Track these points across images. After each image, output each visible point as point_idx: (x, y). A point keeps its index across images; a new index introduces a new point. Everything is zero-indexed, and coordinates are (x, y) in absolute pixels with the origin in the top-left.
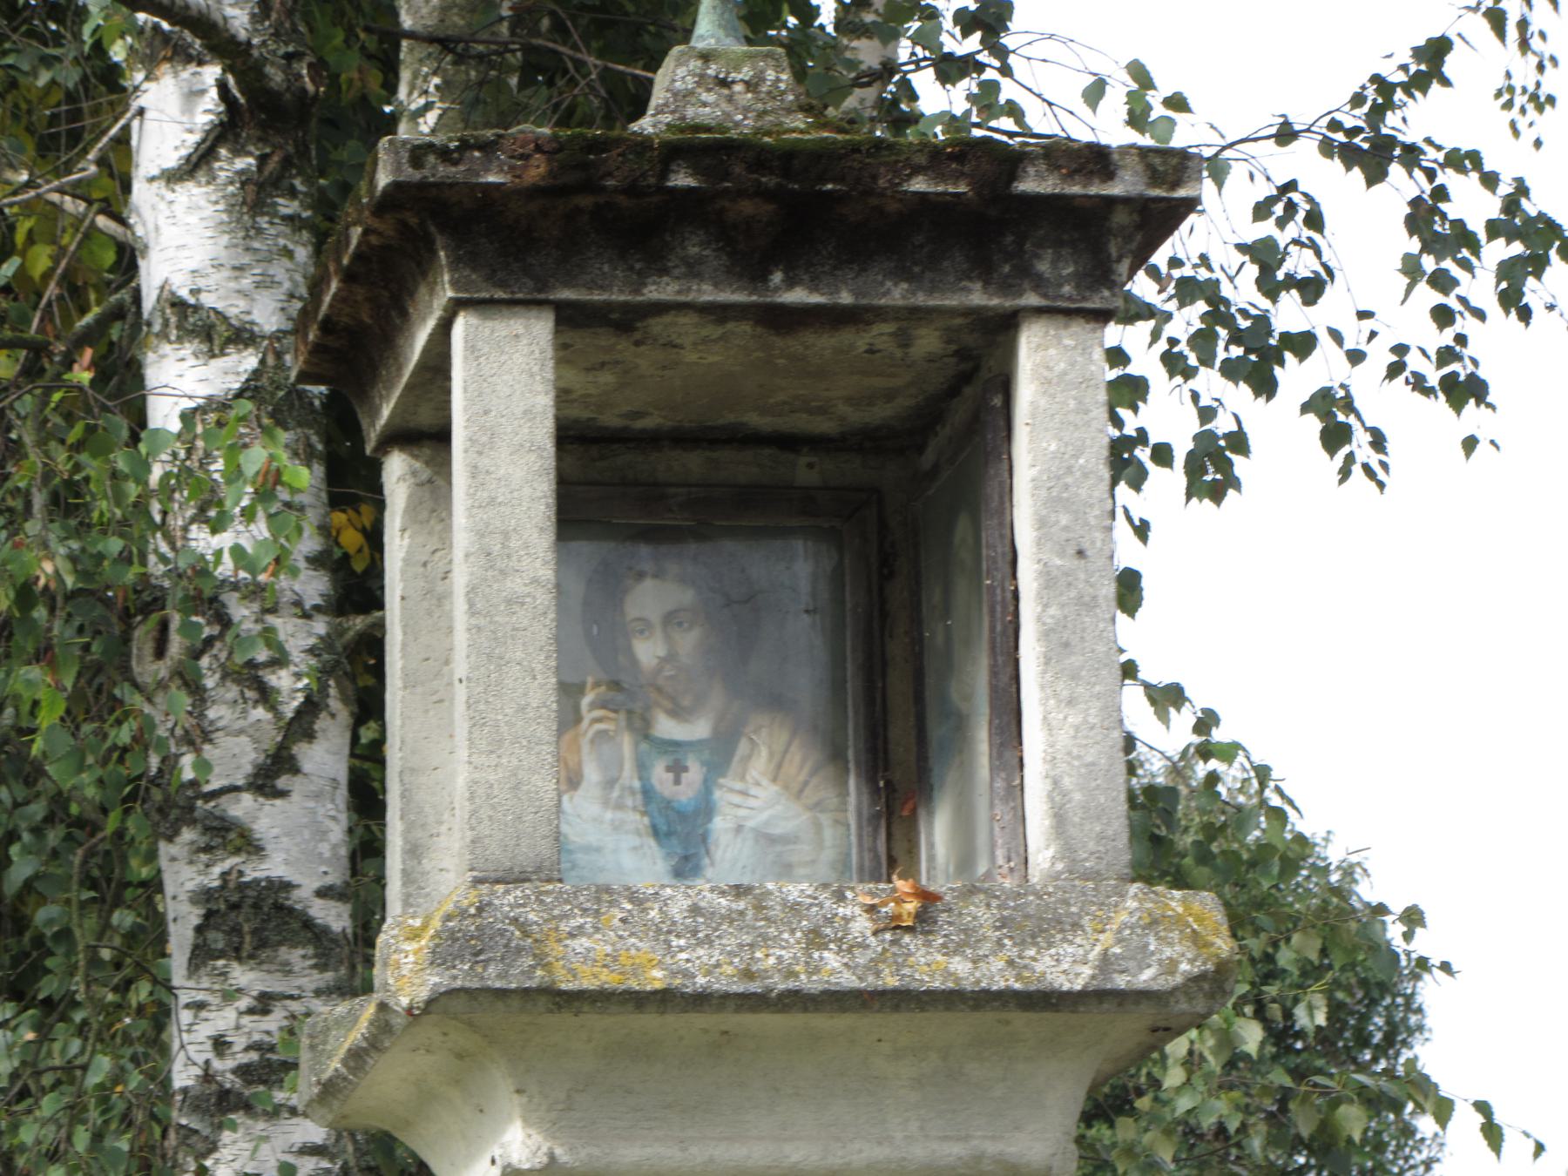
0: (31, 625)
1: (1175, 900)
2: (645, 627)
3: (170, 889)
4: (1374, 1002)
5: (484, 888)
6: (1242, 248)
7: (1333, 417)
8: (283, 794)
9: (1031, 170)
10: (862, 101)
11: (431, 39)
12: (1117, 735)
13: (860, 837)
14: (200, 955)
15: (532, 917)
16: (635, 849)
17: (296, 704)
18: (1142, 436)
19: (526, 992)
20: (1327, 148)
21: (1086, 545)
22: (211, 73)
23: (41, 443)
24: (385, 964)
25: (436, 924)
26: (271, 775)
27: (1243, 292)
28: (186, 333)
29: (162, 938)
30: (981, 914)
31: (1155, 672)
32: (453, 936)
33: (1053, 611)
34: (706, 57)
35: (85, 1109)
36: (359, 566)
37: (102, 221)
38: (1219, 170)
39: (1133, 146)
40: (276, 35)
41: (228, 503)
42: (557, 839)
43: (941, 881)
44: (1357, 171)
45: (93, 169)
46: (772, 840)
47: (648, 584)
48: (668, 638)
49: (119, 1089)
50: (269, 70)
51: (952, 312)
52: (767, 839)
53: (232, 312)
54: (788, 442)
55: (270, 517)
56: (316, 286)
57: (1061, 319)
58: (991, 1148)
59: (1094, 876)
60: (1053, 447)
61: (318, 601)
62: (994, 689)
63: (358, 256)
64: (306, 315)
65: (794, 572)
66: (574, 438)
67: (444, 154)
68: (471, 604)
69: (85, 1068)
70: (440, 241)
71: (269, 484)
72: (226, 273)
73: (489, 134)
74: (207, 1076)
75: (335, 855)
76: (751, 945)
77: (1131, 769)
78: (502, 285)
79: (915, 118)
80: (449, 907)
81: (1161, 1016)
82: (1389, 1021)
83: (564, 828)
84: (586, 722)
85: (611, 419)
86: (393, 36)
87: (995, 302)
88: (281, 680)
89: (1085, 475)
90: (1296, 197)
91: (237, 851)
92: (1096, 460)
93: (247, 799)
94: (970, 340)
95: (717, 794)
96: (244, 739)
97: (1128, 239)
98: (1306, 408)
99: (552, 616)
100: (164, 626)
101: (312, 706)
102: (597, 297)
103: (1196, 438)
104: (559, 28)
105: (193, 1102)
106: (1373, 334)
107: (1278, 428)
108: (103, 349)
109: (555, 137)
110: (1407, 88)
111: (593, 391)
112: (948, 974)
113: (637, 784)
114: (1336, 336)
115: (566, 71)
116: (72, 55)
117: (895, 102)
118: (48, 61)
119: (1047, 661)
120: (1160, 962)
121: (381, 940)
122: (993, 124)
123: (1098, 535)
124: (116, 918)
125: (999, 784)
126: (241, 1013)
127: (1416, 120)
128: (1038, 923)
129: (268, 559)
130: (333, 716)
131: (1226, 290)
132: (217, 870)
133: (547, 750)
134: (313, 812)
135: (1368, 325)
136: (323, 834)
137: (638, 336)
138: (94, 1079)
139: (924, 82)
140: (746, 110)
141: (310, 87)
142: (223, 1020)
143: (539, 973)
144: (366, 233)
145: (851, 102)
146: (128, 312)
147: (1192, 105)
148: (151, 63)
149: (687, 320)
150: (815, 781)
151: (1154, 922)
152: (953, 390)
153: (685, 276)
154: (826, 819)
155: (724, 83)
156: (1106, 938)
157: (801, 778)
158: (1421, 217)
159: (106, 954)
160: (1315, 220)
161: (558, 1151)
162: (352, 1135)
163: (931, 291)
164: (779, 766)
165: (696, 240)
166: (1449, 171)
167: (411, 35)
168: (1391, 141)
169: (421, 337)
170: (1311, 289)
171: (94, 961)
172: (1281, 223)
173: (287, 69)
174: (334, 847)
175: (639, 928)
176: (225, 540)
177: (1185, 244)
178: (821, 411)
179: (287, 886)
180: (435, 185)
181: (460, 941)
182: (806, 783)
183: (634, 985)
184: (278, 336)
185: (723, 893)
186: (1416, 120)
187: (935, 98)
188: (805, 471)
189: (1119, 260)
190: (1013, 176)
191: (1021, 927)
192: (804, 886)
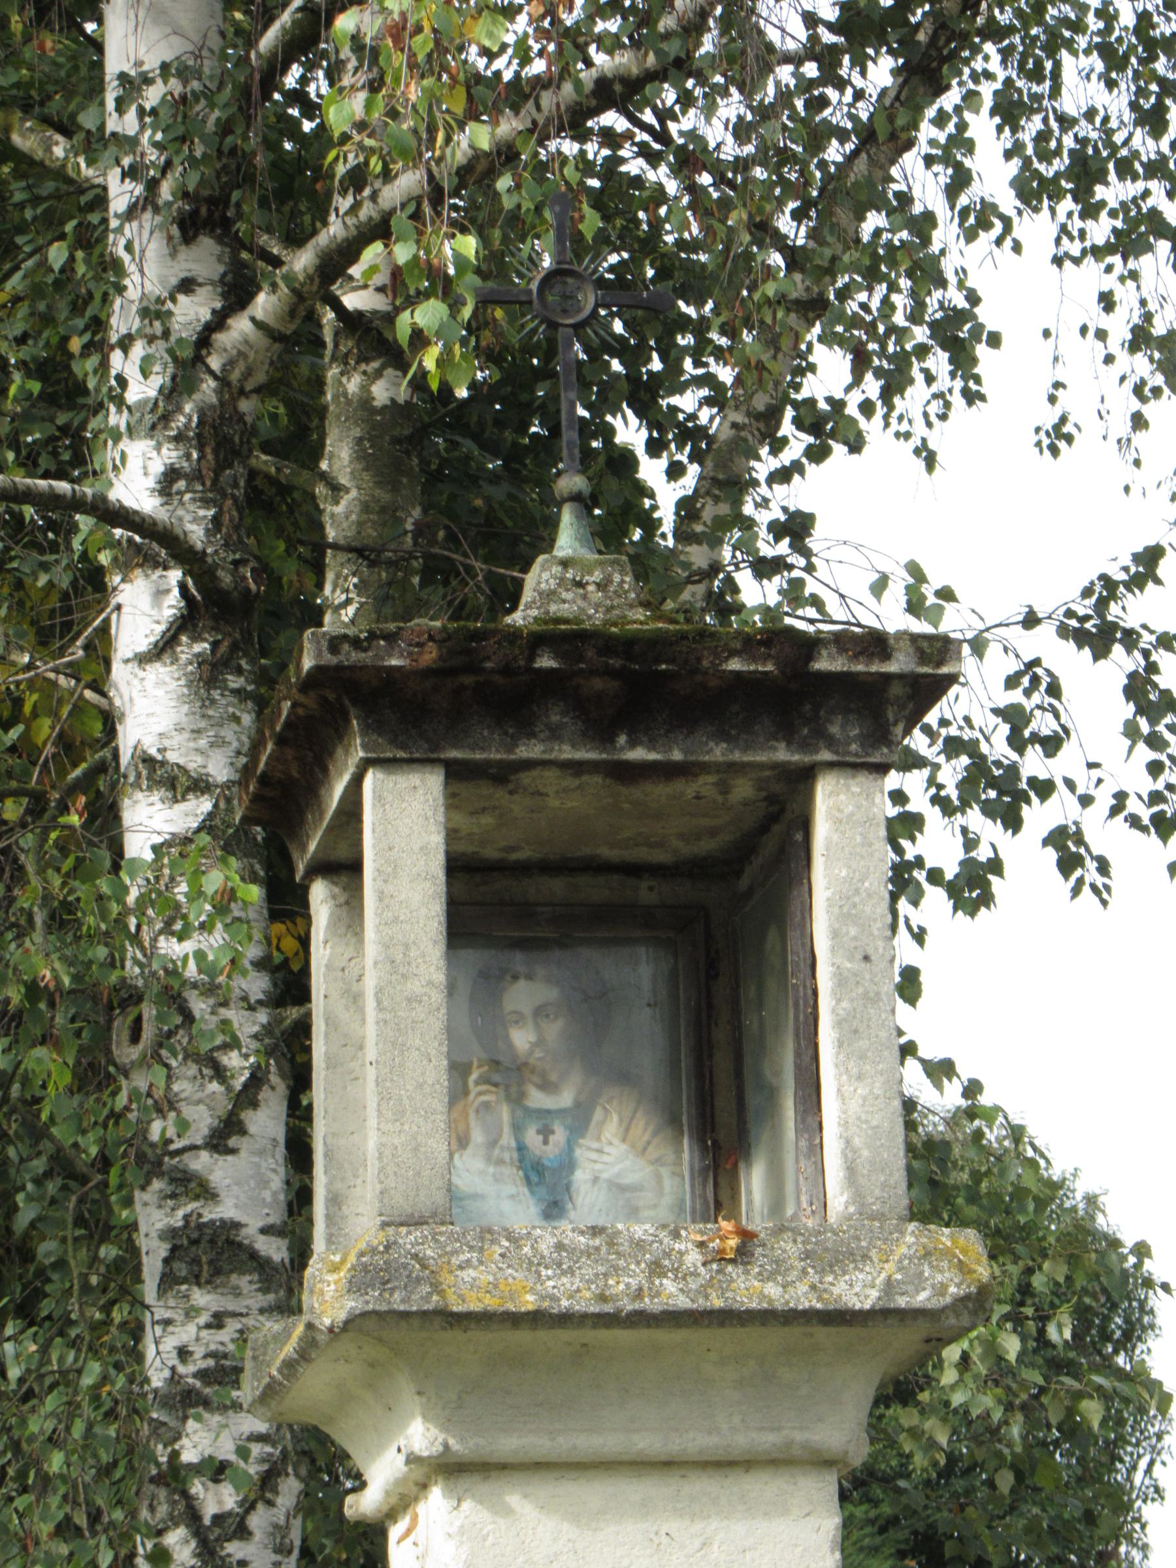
0: (37, 1015)
1: (945, 1236)
2: (519, 1019)
3: (143, 1228)
4: (1114, 1306)
5: (391, 1230)
6: (996, 711)
7: (1068, 849)
8: (233, 1151)
9: (824, 653)
10: (693, 594)
11: (349, 549)
12: (897, 1103)
13: (692, 1186)
14: (168, 1281)
15: (429, 1252)
16: (512, 1197)
17: (243, 1079)
18: (919, 862)
19: (424, 1314)
20: (1063, 632)
21: (870, 951)
22: (175, 575)
23: (41, 871)
24: (312, 1292)
25: (352, 1259)
26: (223, 1138)
27: (998, 748)
28: (155, 783)
29: (138, 1269)
30: (789, 1248)
31: (929, 1050)
32: (365, 1269)
33: (845, 1004)
34: (565, 563)
35: (79, 1406)
36: (296, 967)
37: (88, 694)
38: (978, 646)
39: (905, 633)
40: (226, 545)
41: (192, 917)
42: (449, 1190)
43: (758, 1220)
44: (1087, 649)
45: (81, 653)
46: (622, 1188)
47: (522, 984)
48: (537, 1027)
49: (107, 1388)
50: (221, 573)
51: (761, 766)
52: (618, 1188)
53: (191, 766)
54: (633, 870)
55: (226, 926)
56: (256, 746)
57: (849, 771)
58: (799, 1437)
59: (880, 1217)
60: (844, 873)
61: (261, 996)
62: (798, 1067)
63: (288, 724)
64: (247, 771)
65: (639, 975)
66: (462, 868)
67: (356, 643)
68: (379, 1002)
69: (79, 1372)
70: (353, 712)
71: (225, 901)
72: (186, 735)
73: (392, 626)
74: (174, 1377)
75: (275, 1200)
76: (605, 1275)
77: (910, 1126)
78: (403, 747)
79: (739, 608)
80: (362, 1245)
81: (934, 1328)
82: (1127, 1320)
83: (455, 1180)
84: (472, 1096)
85: (491, 853)
86: (320, 547)
87: (796, 758)
88: (232, 1059)
89: (870, 896)
90: (1039, 671)
91: (197, 1197)
92: (878, 883)
93: (204, 1155)
94: (777, 788)
95: (578, 1152)
96: (202, 1107)
97: (902, 707)
98: (1046, 842)
99: (443, 1011)
100: (138, 1020)
101: (256, 1080)
102: (478, 756)
103: (962, 863)
104: (451, 538)
105: (165, 1400)
106: (1100, 781)
107: (1024, 855)
108: (92, 795)
109: (444, 628)
110: (1128, 585)
111: (476, 830)
112: (762, 1296)
113: (513, 1144)
114: (1070, 784)
115: (458, 574)
116: (64, 562)
117: (721, 594)
118: (45, 567)
119: (840, 1044)
120: (933, 1286)
121: (308, 1272)
122: (800, 612)
123: (881, 944)
124: (102, 1252)
125: (803, 1143)
126: (200, 1328)
127: (1132, 611)
128: (834, 1256)
129: (225, 961)
130: (273, 1088)
131: (984, 748)
132: (180, 1213)
133: (440, 1119)
134: (258, 1166)
135: (1095, 773)
136: (264, 1183)
137: (511, 786)
138: (87, 1381)
139: (744, 578)
140: (597, 606)
141: (253, 587)
142: (186, 1333)
143: (435, 1298)
144: (294, 706)
145: (686, 596)
146: (108, 767)
147: (958, 595)
148: (125, 567)
149: (551, 774)
150: (656, 1141)
151: (927, 1254)
152: (764, 828)
153: (549, 739)
154: (665, 1172)
155: (580, 585)
156: (890, 1267)
157: (646, 1138)
158: (1137, 688)
159: (94, 1280)
160: (1054, 690)
161: (451, 1442)
162: (290, 1426)
163: (745, 750)
164: (627, 1130)
165: (556, 709)
166: (1161, 651)
167: (335, 546)
168: (1114, 626)
169: (338, 789)
170: (1051, 745)
171: (86, 1288)
172: (1028, 693)
173: (234, 573)
174: (274, 1194)
175: (520, 1259)
176: (189, 946)
177: (951, 708)
178: (661, 844)
179: (237, 1225)
180: (349, 668)
181: (366, 1276)
182: (649, 1143)
183: (511, 1307)
184: (228, 785)
185: (582, 1233)
186: (1132, 611)
187: (755, 593)
188: (646, 892)
189: (895, 723)
190: (810, 657)
191: (821, 1259)
192: (647, 1226)
